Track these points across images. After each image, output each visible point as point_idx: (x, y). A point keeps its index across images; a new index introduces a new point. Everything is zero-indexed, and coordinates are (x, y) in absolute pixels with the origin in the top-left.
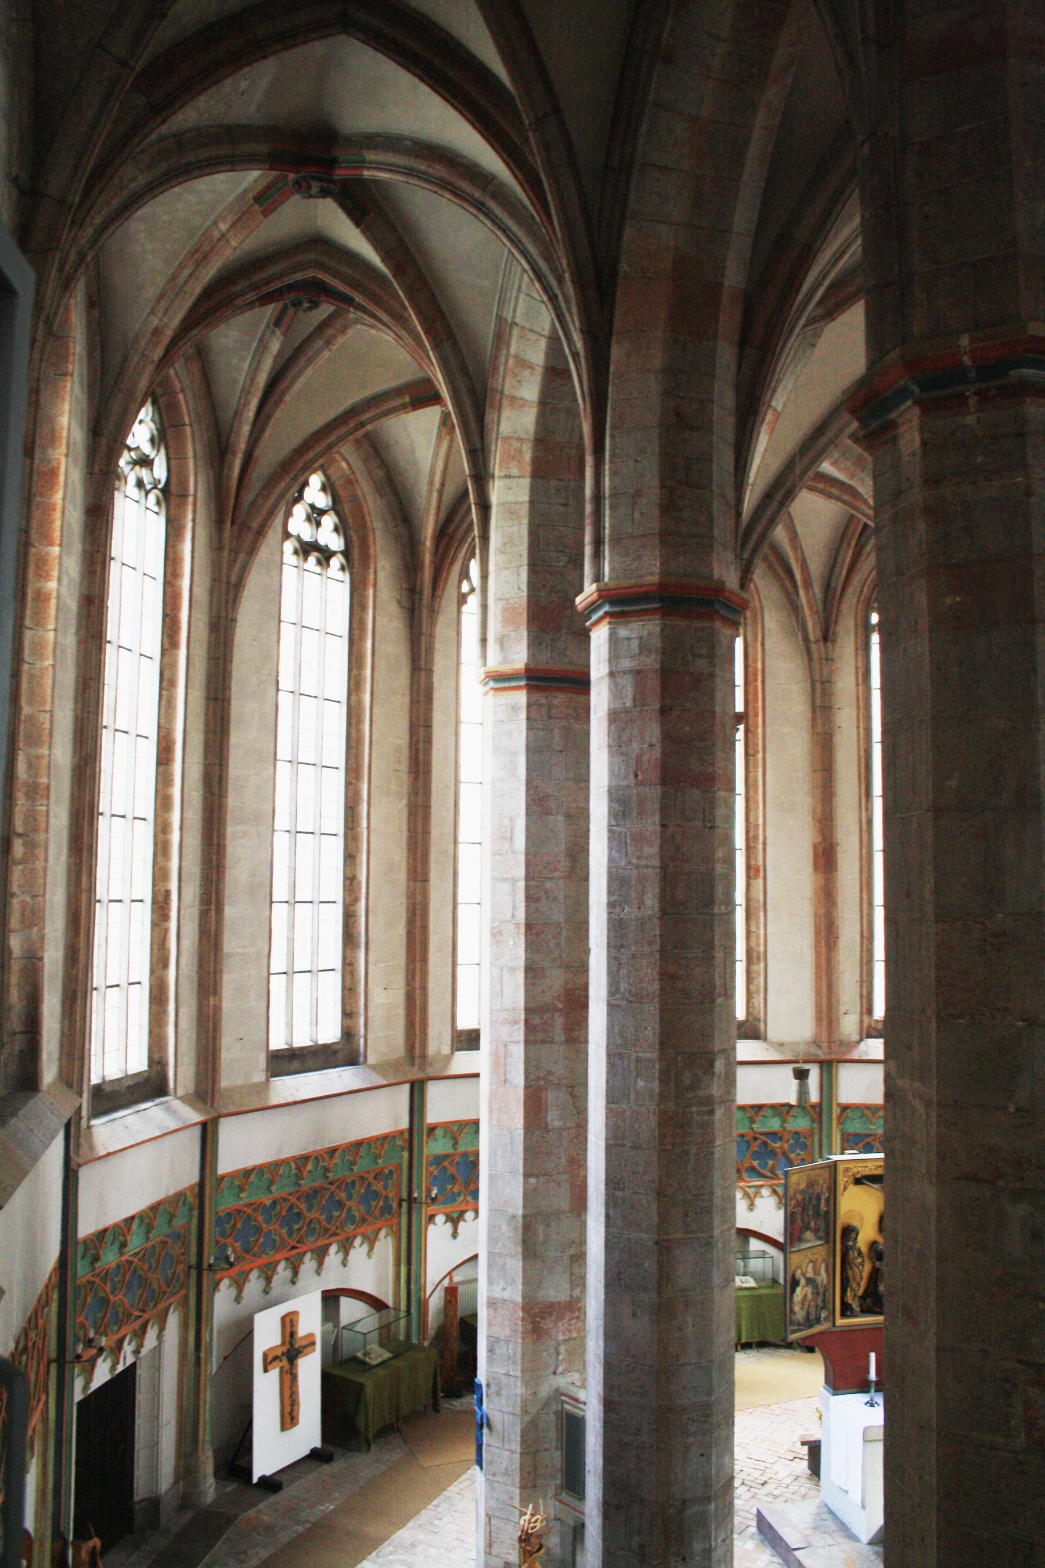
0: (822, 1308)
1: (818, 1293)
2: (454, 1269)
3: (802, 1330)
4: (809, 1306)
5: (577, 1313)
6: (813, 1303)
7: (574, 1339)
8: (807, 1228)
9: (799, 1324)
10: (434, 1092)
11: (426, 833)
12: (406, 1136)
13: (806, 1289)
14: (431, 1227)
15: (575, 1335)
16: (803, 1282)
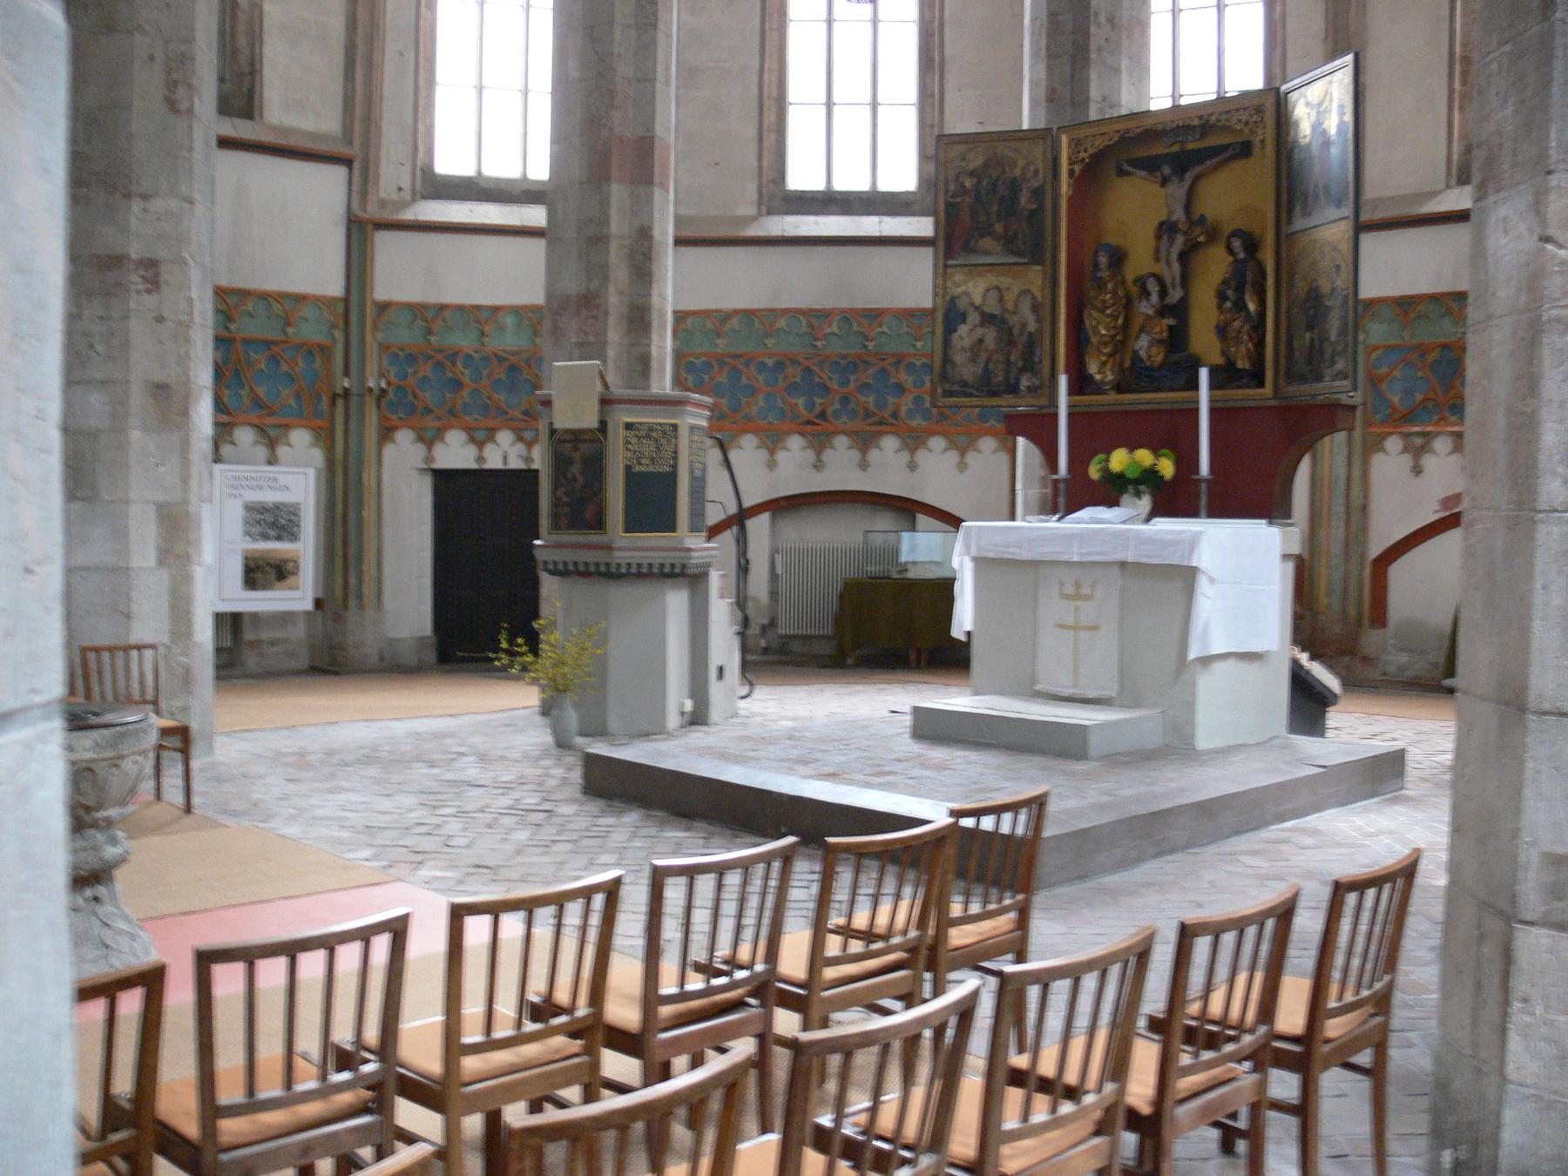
0: (1022, 370)
1: (1012, 343)
2: (514, 881)
3: (971, 395)
4: (989, 360)
5: (595, 312)
6: (998, 357)
7: (589, 343)
8: (986, 231)
9: (964, 384)
10: (388, 249)
11: (222, 21)
12: (340, 309)
13: (980, 331)
14: (389, 450)
15: (591, 339)
16: (973, 318)
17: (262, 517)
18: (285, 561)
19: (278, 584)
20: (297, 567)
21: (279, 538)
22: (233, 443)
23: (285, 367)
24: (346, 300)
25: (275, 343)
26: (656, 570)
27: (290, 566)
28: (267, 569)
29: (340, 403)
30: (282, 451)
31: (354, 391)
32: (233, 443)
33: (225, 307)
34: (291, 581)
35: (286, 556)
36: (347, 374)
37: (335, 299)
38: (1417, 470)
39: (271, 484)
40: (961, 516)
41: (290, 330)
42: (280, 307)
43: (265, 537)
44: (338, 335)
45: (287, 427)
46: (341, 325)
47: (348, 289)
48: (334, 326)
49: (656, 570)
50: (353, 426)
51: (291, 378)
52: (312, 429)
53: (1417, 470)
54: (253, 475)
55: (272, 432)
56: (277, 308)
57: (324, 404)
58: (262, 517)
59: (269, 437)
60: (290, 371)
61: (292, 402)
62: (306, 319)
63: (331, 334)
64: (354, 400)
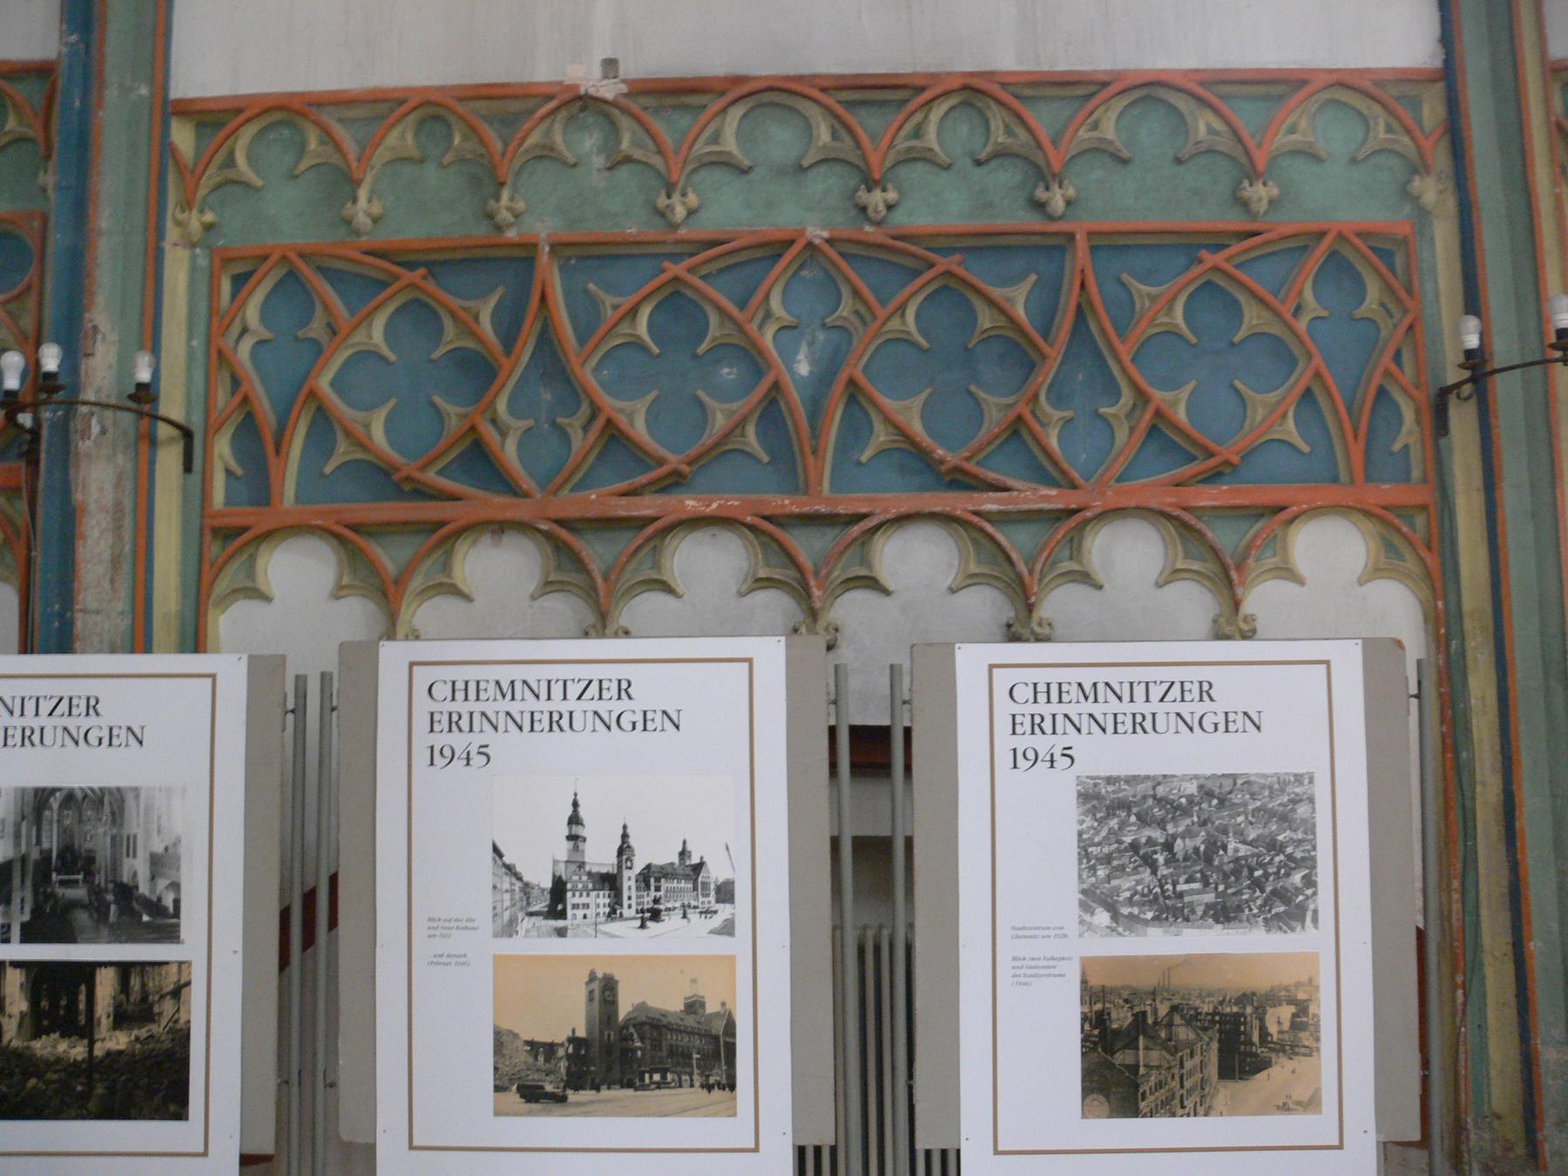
12: (1432, 112)
17: (1158, 835)
18: (1260, 1002)
19: (1225, 1092)
20: (1303, 1019)
21: (1224, 913)
22: (1085, 578)
23: (1253, 317)
24: (1448, 75)
25: (1217, 240)
27: (1278, 1019)
28: (1184, 1033)
29: (1462, 419)
30: (1261, 598)
32: (1085, 578)
33: (1023, 135)
34: (1280, 1072)
35: (1261, 982)
36: (1473, 303)
37: (1406, 78)
38: (702, 858)
39: (78, 723)
41: (1260, 193)
42: (1218, 125)
43: (1170, 910)
44: (1432, 190)
45: (1277, 514)
46: (1441, 159)
47: (1448, 38)
48: (1420, 167)
50: (1513, 499)
51: (1282, 353)
52: (1367, 513)
53: (702, 858)
54: (533, 674)
55: (1225, 536)
56: (1203, 124)
57: (1409, 431)
59: (1215, 552)
60: (1276, 329)
61: (1290, 429)
62: (1309, 154)
63: (1405, 194)
64: (1505, 389)
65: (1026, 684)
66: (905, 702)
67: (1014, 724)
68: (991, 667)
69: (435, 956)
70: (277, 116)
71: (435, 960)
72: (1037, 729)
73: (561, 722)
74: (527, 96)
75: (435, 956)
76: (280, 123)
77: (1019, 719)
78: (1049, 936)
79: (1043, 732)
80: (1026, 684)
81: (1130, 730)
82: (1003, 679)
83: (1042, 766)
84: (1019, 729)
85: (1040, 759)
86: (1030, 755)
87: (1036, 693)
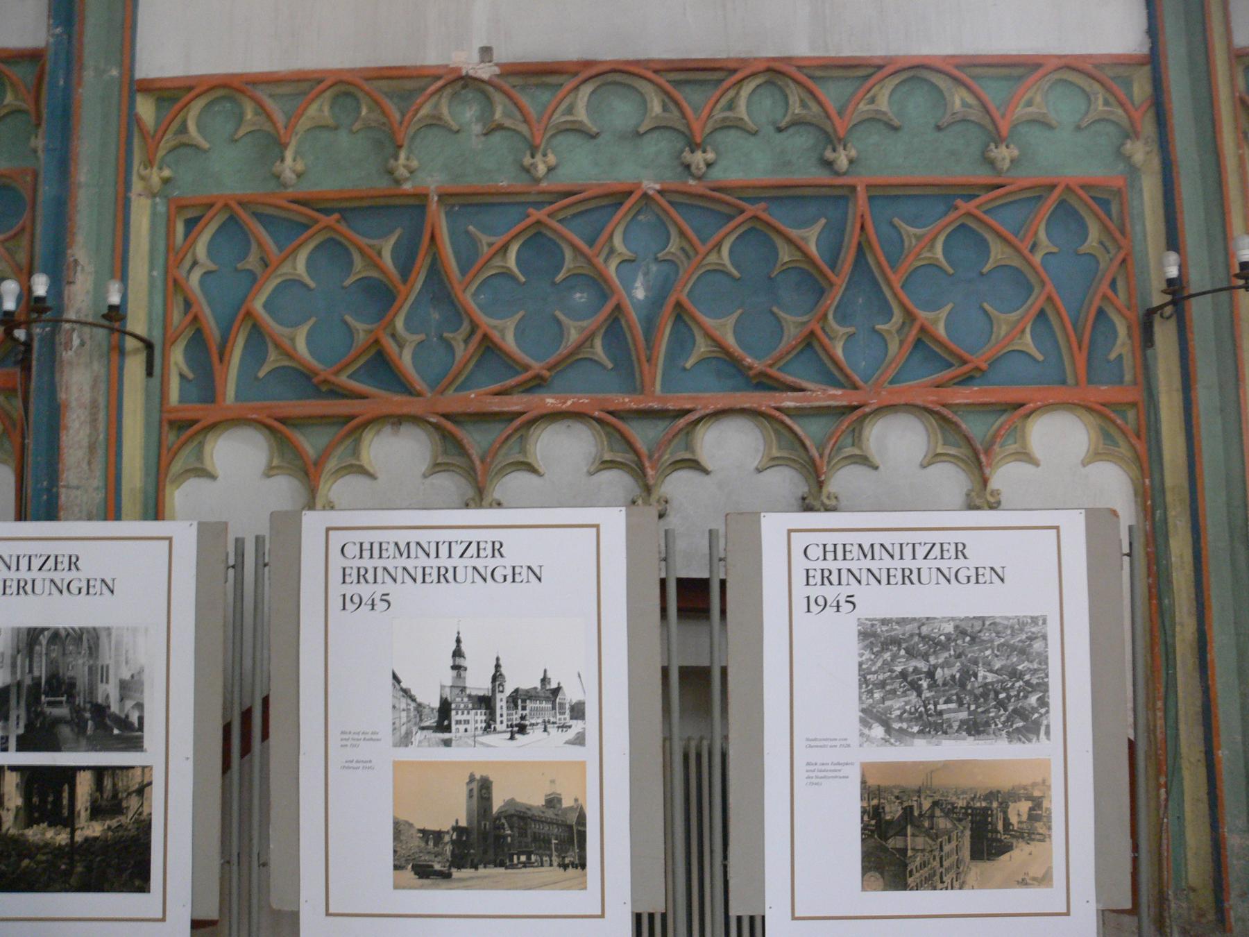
12: (1141, 89)
17: (922, 665)
18: (1004, 798)
19: (976, 870)
20: (1038, 812)
21: (975, 728)
22: (865, 460)
23: (998, 253)
24: (1154, 60)
25: (970, 191)
26: (315, 380)
27: (1018, 812)
28: (943, 823)
29: (1165, 334)
30: (1005, 476)
31: (1197, 280)
32: (865, 460)
33: (815, 108)
35: (1004, 783)
36: (1173, 241)
37: (1120, 62)
38: (559, 684)
40: (1127, 741)
41: (1004, 154)
43: (932, 725)
44: (1141, 152)
45: (1017, 409)
46: (1148, 127)
47: (1153, 31)
48: (1131, 133)
49: (315, 380)
50: (1205, 397)
51: (1021, 282)
52: (1089, 409)
53: (559, 684)
55: (976, 427)
56: (958, 99)
57: (1123, 343)
58: (922, 665)
59: (968, 440)
60: (1016, 262)
61: (1027, 342)
62: (1043, 123)
63: (1119, 154)
64: (1199, 310)
65: (818, 545)
66: (721, 560)
67: (808, 577)
68: (790, 531)
69: (346, 762)
70: (220, 93)
71: (347, 765)
72: (826, 581)
73: (447, 575)
74: (419, 77)
75: (346, 762)
76: (223, 98)
77: (811, 573)
78: (835, 746)
79: (831, 584)
80: (818, 545)
81: (900, 582)
82: (799, 541)
83: (830, 610)
84: (812, 581)
85: (828, 605)
86: (821, 601)
87: (825, 552)
